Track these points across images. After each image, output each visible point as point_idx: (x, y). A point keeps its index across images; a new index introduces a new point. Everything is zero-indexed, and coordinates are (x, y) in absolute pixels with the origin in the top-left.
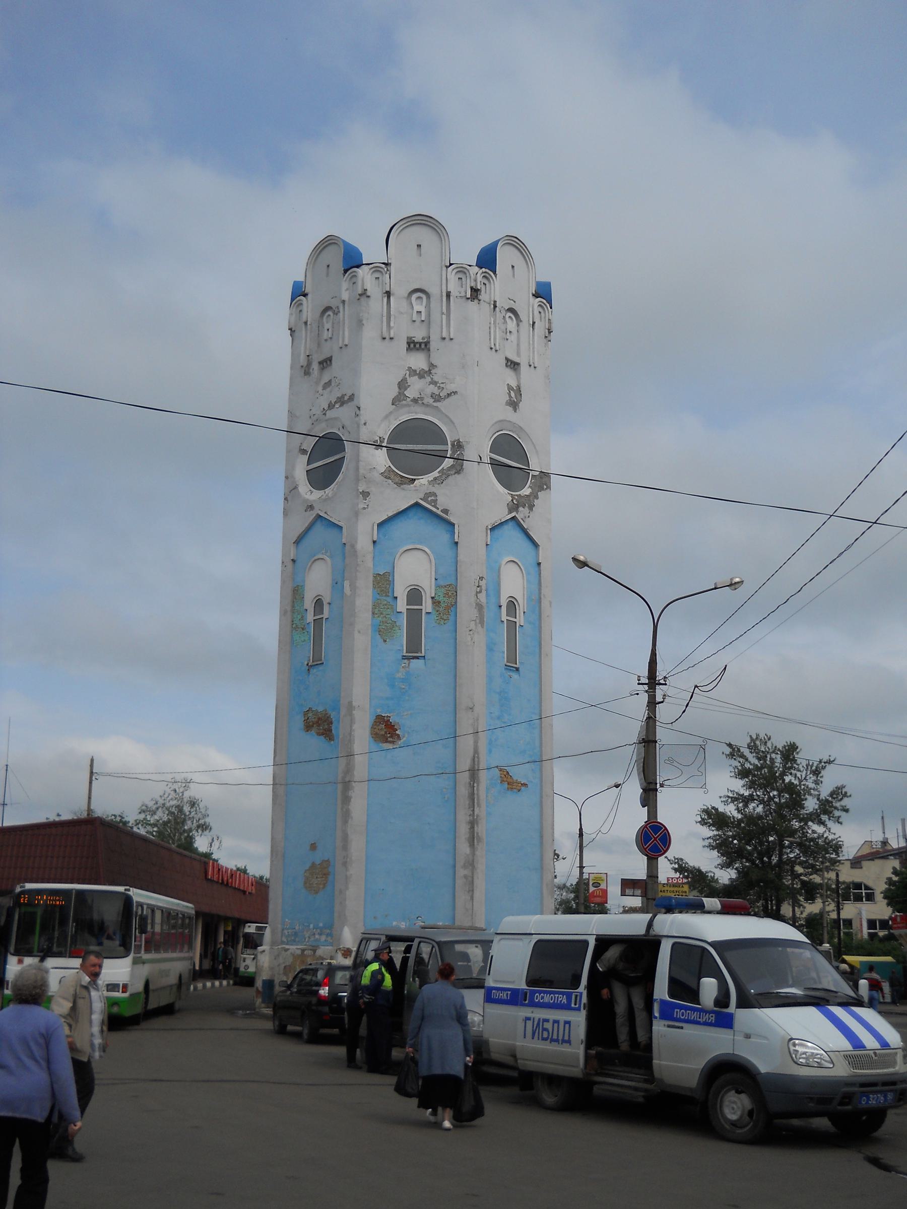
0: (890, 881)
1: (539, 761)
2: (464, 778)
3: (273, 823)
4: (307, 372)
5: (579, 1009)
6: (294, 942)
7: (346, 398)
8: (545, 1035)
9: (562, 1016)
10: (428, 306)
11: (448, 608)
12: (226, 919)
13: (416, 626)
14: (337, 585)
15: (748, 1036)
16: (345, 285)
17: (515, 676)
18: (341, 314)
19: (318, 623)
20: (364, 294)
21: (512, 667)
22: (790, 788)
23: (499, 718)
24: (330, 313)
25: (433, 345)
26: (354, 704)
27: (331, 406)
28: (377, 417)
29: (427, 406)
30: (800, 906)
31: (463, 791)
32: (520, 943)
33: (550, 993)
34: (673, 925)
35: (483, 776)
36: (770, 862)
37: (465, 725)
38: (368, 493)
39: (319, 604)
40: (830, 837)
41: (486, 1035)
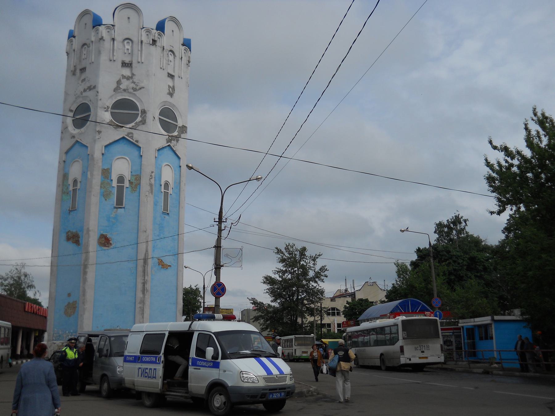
0: (345, 307)
1: (177, 254)
2: (141, 263)
3: (50, 285)
4: (74, 73)
5: (160, 363)
6: (58, 340)
8: (146, 375)
9: (152, 366)
10: (132, 47)
12: (35, 330)
13: (120, 194)
14: (84, 173)
15: (225, 371)
16: (93, 34)
17: (167, 217)
18: (91, 48)
19: (74, 191)
20: (102, 39)
21: (166, 212)
22: (303, 267)
23: (158, 236)
24: (86, 46)
25: (134, 65)
26: (90, 229)
28: (106, 96)
29: (130, 93)
30: (305, 318)
31: (140, 269)
32: (139, 335)
33: (149, 357)
34: (200, 325)
35: (150, 262)
36: (293, 299)
37: (142, 237)
39: (75, 182)
40: (320, 288)
41: (124, 377)
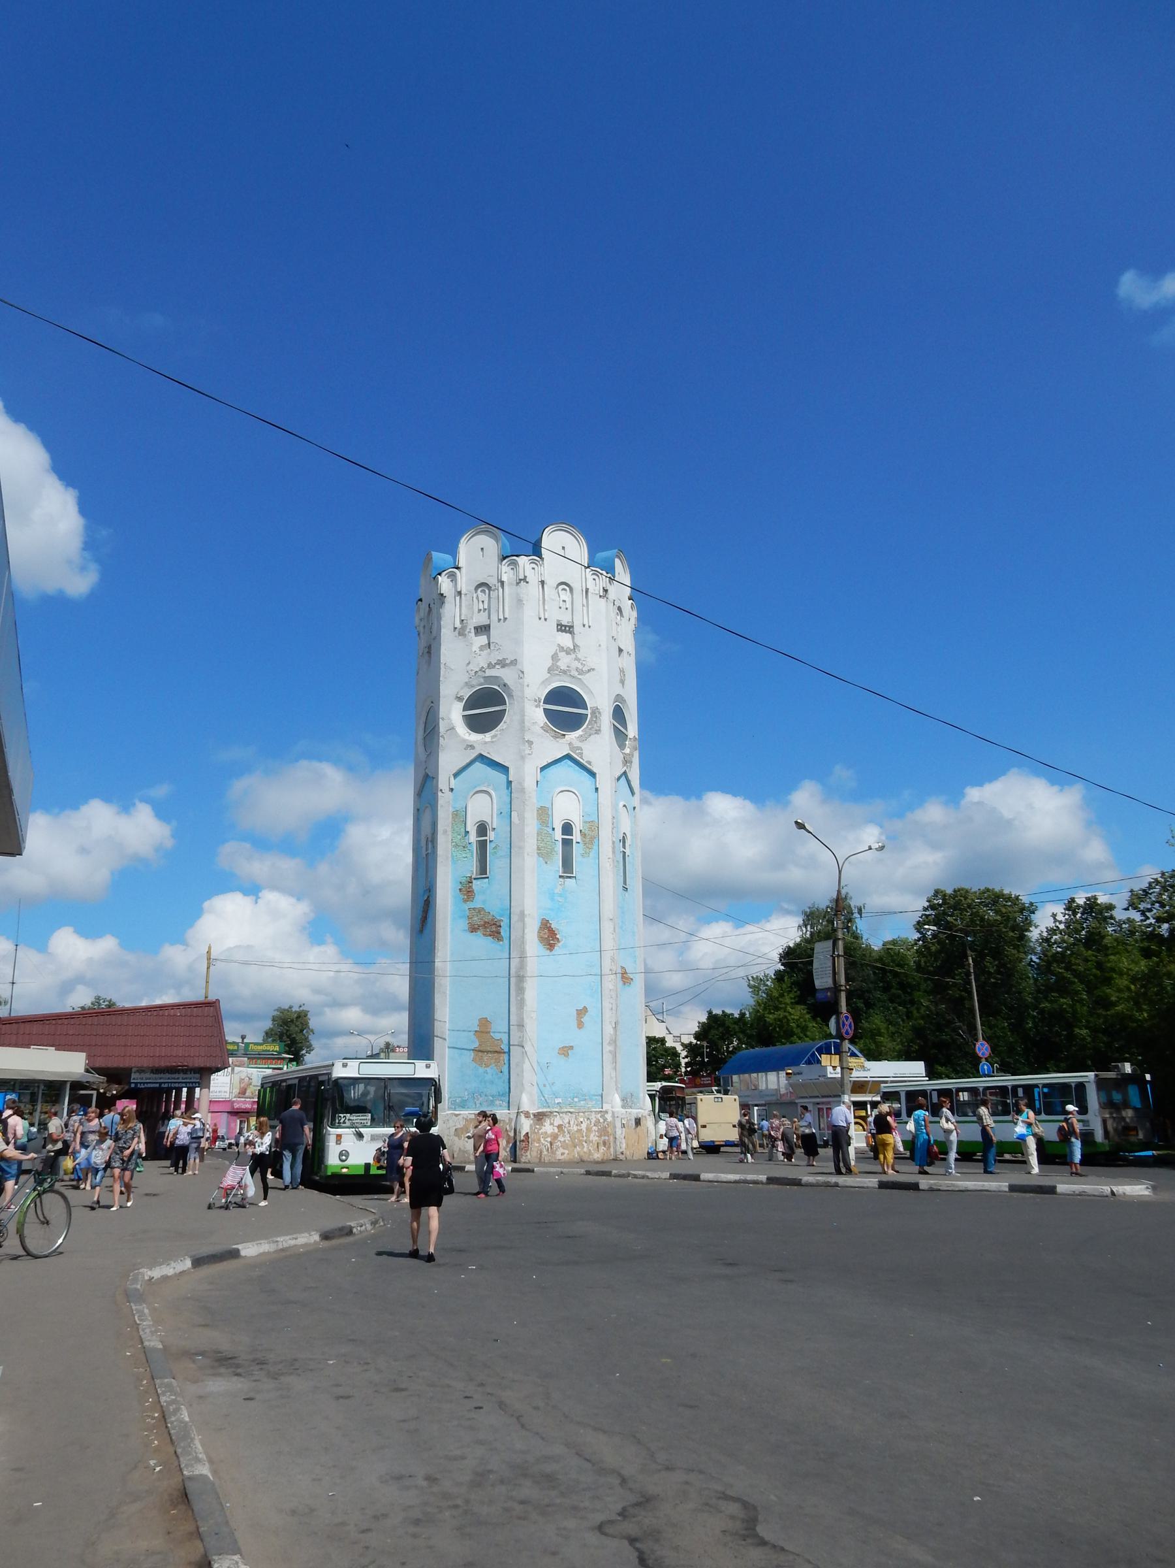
11: (592, 838)
14: (508, 813)
20: (525, 580)
25: (576, 630)
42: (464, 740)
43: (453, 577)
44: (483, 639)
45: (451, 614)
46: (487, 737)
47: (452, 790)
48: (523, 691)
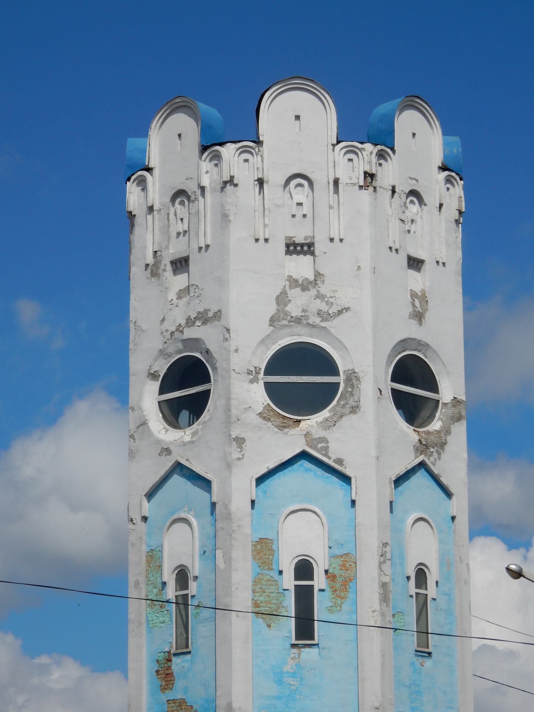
7: (210, 314)
14: (208, 554)
17: (428, 663)
20: (231, 181)
25: (318, 248)
27: (190, 322)
28: (203, 245)
38: (243, 440)
39: (182, 576)
42: (158, 442)
43: (142, 182)
44: (180, 281)
45: (146, 240)
46: (185, 435)
47: (145, 519)
48: (228, 360)
